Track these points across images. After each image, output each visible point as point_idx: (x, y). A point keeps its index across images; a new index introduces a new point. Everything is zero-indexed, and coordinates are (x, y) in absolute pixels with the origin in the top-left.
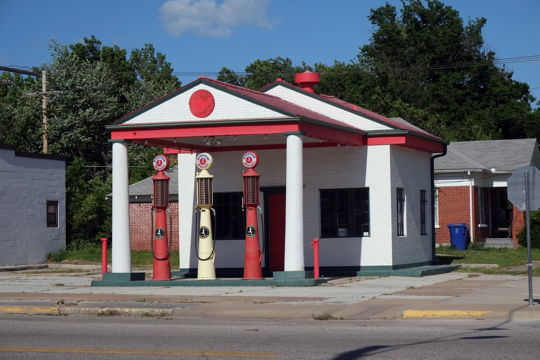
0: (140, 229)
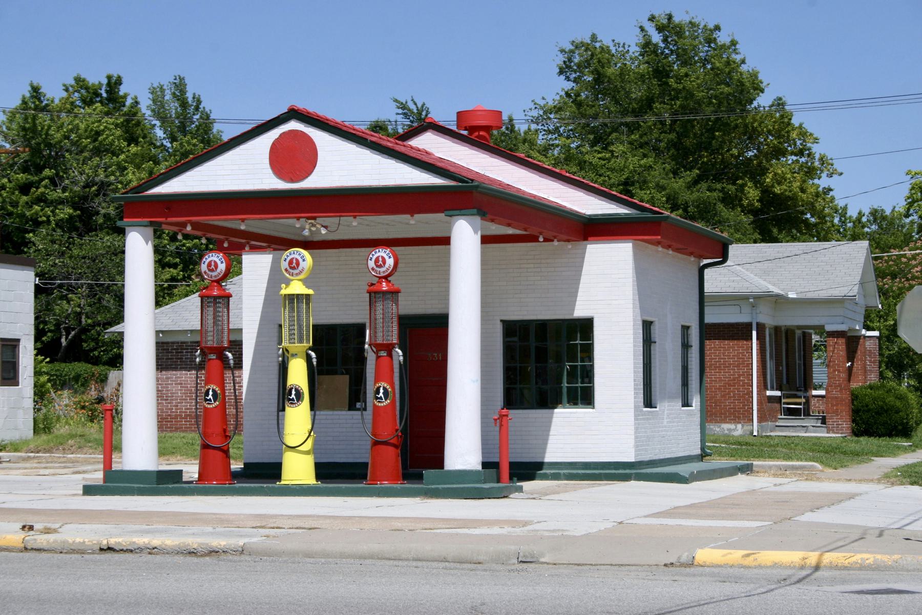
0: (167, 391)
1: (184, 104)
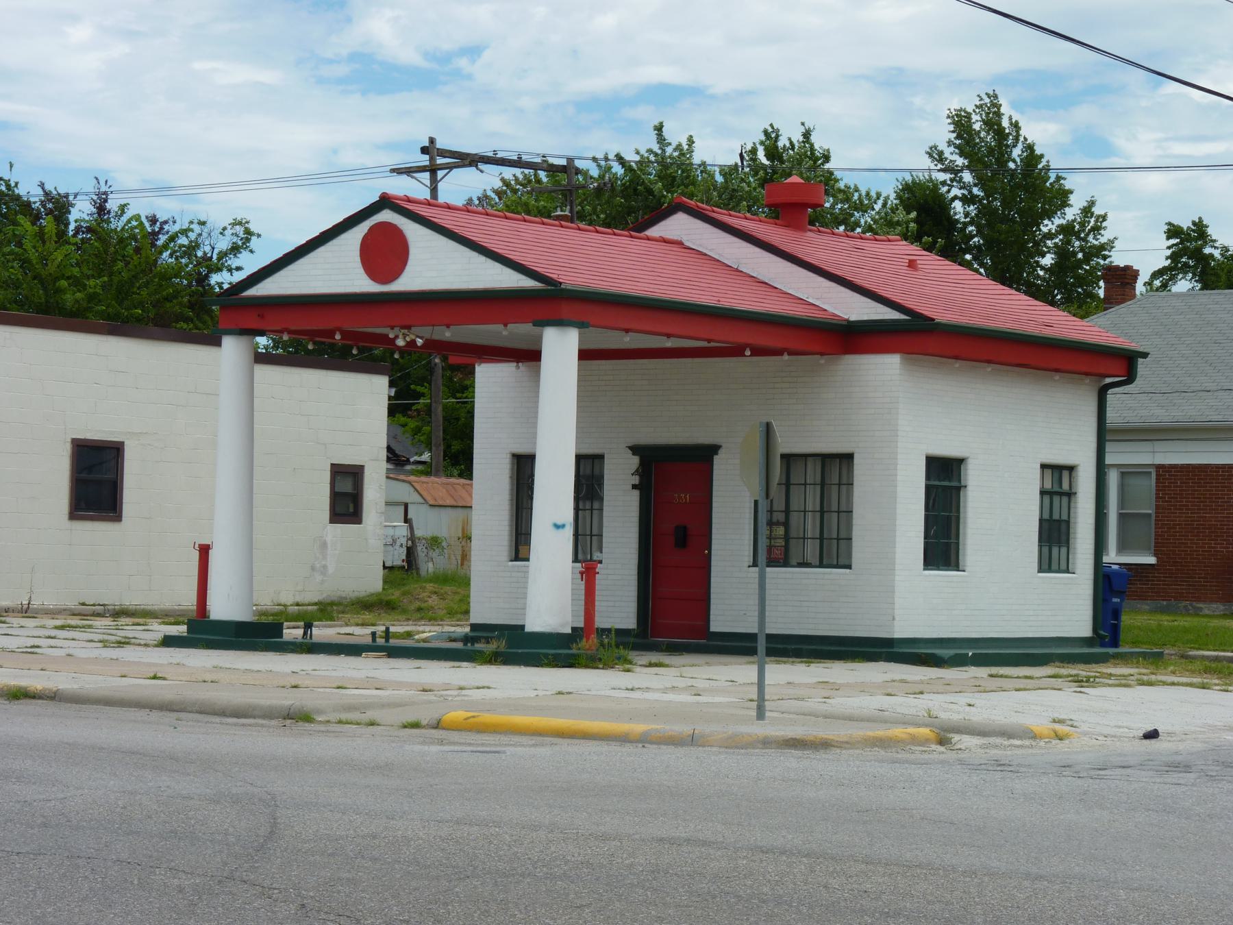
1: (1000, 134)
